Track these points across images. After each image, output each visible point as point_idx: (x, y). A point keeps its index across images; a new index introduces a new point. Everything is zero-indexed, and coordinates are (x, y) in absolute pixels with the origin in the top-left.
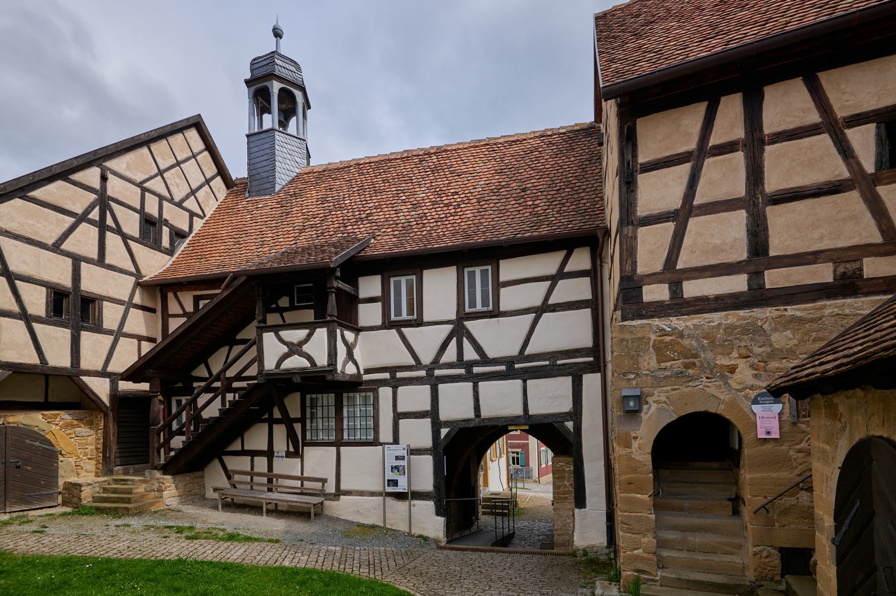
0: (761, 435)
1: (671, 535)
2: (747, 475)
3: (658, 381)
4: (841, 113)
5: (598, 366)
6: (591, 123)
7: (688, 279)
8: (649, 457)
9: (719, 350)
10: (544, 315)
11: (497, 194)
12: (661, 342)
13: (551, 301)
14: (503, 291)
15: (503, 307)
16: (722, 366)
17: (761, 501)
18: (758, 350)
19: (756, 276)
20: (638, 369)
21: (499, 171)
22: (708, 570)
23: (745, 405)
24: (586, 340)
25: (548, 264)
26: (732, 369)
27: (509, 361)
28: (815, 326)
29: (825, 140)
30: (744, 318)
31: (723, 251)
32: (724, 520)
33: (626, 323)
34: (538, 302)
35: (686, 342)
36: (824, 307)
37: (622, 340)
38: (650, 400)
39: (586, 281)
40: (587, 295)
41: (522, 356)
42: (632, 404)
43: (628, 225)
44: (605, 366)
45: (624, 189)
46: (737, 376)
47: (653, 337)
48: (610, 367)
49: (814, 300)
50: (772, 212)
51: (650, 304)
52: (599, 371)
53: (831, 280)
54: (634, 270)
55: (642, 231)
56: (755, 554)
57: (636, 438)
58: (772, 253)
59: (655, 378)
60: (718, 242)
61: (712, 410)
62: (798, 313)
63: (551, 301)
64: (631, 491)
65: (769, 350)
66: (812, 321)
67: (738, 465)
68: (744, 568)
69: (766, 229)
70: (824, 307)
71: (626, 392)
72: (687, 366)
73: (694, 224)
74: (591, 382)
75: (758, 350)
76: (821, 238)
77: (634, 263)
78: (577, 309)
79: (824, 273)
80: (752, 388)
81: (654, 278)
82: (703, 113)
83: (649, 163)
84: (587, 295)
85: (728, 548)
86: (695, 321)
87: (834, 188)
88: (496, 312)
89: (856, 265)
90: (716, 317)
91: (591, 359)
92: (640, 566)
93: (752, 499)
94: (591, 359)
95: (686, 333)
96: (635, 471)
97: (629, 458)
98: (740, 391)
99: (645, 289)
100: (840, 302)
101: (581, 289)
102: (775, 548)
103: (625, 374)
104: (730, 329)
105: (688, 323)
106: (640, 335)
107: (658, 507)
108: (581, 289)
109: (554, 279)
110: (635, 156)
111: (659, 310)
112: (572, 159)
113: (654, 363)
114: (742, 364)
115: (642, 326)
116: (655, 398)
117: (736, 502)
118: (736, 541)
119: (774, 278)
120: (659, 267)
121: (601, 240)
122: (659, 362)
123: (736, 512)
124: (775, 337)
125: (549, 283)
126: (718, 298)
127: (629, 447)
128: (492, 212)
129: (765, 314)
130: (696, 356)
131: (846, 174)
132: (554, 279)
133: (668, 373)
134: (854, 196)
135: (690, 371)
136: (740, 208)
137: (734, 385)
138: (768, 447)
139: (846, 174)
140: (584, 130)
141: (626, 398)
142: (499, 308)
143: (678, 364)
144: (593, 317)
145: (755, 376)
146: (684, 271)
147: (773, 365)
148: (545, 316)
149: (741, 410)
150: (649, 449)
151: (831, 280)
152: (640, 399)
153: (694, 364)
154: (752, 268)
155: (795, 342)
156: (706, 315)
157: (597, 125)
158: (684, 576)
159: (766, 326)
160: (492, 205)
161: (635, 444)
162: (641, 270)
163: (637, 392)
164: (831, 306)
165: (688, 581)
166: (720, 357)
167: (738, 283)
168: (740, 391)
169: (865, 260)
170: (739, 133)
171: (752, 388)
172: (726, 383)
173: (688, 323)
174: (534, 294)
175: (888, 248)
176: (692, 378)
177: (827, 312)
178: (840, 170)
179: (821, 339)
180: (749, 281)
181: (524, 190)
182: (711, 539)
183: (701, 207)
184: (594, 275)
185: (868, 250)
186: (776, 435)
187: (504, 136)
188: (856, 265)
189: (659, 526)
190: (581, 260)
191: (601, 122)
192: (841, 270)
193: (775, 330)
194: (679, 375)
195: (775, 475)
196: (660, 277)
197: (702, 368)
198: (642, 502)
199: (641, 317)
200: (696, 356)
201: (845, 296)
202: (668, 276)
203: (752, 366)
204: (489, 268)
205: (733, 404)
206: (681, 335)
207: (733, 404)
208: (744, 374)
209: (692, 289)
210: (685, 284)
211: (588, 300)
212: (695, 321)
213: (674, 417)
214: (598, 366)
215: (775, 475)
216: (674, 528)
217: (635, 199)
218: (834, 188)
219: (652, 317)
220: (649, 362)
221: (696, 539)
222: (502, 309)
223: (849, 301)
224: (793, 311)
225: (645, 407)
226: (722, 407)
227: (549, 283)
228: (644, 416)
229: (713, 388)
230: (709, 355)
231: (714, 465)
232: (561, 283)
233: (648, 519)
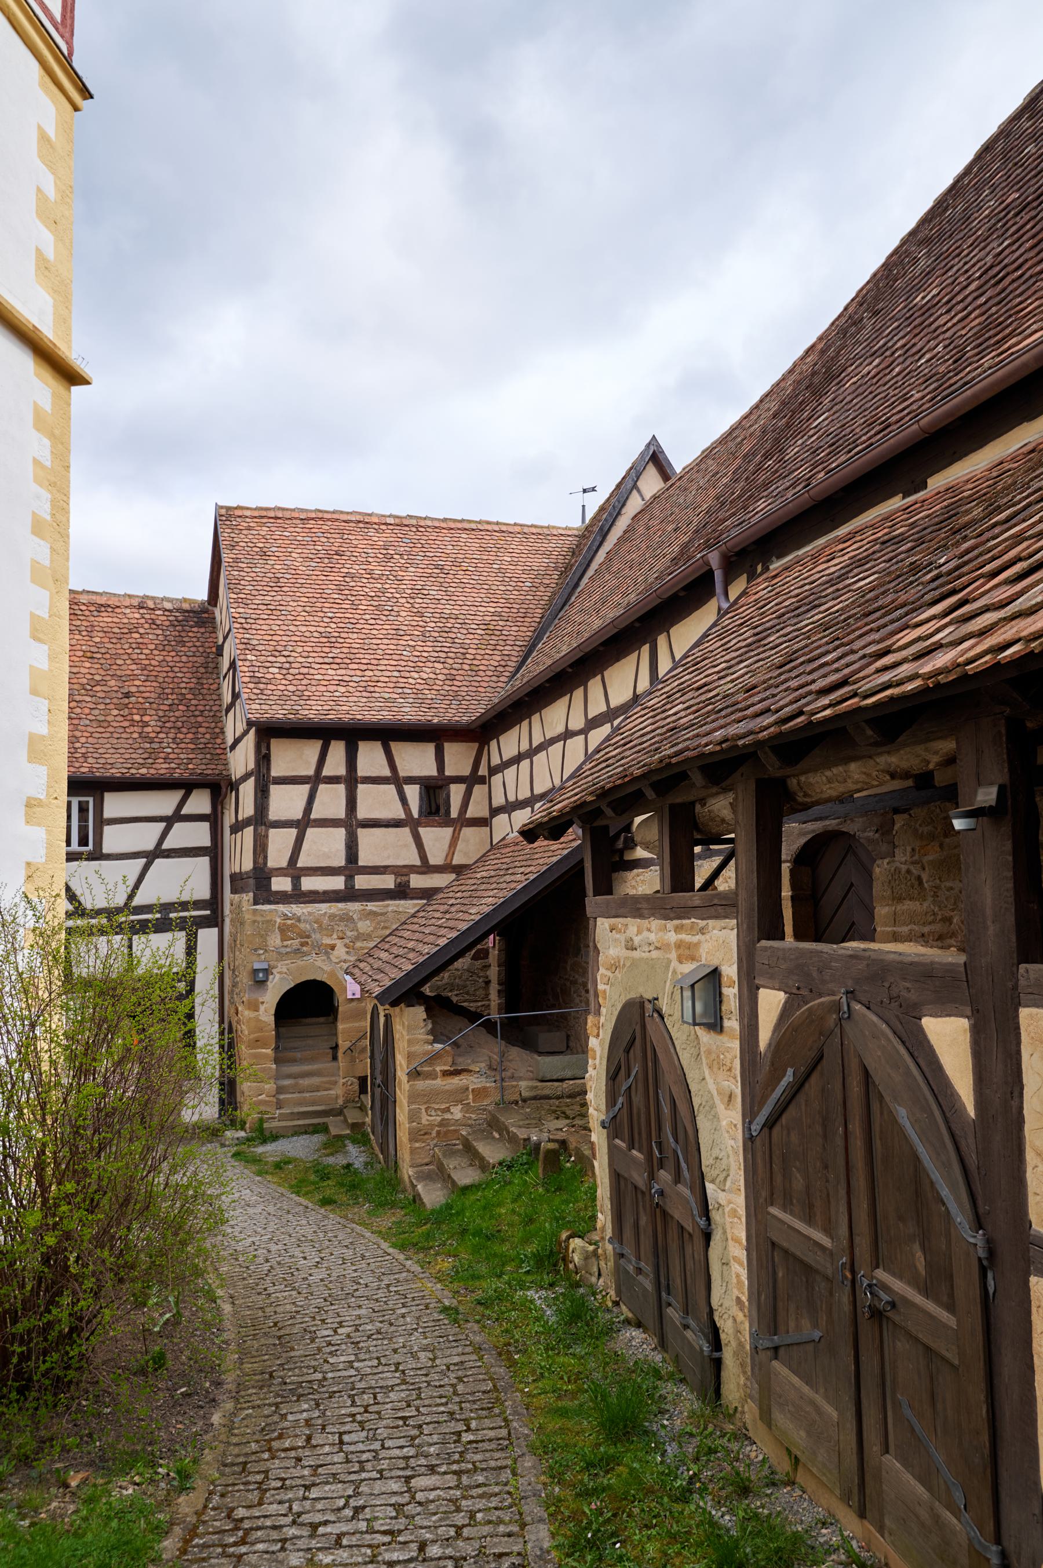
0: (350, 996)
1: (287, 1082)
2: (341, 1026)
3: (281, 956)
4: (402, 773)
5: (215, 920)
6: (203, 603)
7: (305, 875)
8: (273, 1018)
9: (325, 932)
10: (157, 861)
11: (91, 693)
12: (284, 924)
13: (165, 846)
14: (107, 830)
15: (106, 850)
16: (327, 945)
17: (348, 1044)
18: (349, 934)
19: (350, 879)
20: (266, 946)
21: (89, 654)
22: (313, 1104)
23: (340, 974)
24: (204, 892)
25: (164, 803)
26: (333, 947)
27: (110, 913)
28: (383, 918)
29: (392, 788)
30: (342, 910)
31: (329, 857)
32: (327, 1065)
33: (258, 907)
34: (150, 845)
35: (302, 926)
36: (388, 906)
37: (254, 921)
38: (274, 971)
39: (205, 826)
40: (206, 842)
41: (127, 907)
42: (261, 975)
43: (262, 824)
44: (223, 921)
45: (259, 795)
46: (335, 952)
47: (278, 920)
48: (227, 921)
49: (383, 900)
50: (361, 833)
51: (277, 892)
52: (216, 926)
53: (392, 887)
54: (265, 863)
55: (272, 832)
56: (344, 1084)
57: (263, 1003)
58: (360, 863)
59: (279, 953)
60: (326, 850)
61: (319, 979)
62: (374, 909)
63: (165, 846)
64: (258, 1048)
65: (355, 933)
66: (382, 914)
67: (336, 1019)
68: (337, 1097)
69: (357, 845)
70: (388, 906)
71: (257, 966)
72: (302, 945)
73: (311, 833)
74: (208, 937)
75: (349, 934)
76: (389, 857)
77: (266, 858)
78: (195, 856)
79: (388, 882)
80: (345, 961)
81: (280, 872)
82: (319, 749)
83: (279, 777)
84: (206, 842)
85: (327, 1086)
86: (309, 909)
87: (396, 824)
88: (97, 855)
89: (406, 878)
90: (324, 907)
91: (208, 912)
92: (262, 1108)
93: (344, 1044)
94: (208, 912)
95: (302, 918)
96: (261, 1030)
97: (258, 1020)
98: (337, 963)
99: (273, 880)
100: (397, 902)
101: (199, 835)
102: (355, 1077)
103: (256, 950)
104: (332, 917)
105: (304, 911)
106: (268, 918)
107: (276, 1061)
108: (199, 835)
109: (170, 821)
110: (269, 769)
111: (283, 898)
112: (184, 659)
113: (278, 942)
114: (339, 943)
115: (271, 911)
116: (279, 969)
117: (335, 1048)
118: (333, 1079)
119: (362, 882)
120: (284, 864)
121: (224, 790)
122: (282, 940)
123: (335, 1058)
124: (360, 925)
125: (164, 824)
126: (325, 892)
127: (257, 1011)
128: (88, 722)
129: (354, 907)
130: (308, 937)
131: (403, 816)
132: (170, 821)
133: (288, 950)
134: (406, 831)
135: (305, 949)
136: (341, 826)
137: (334, 960)
138: (354, 1004)
139: (403, 816)
140: (194, 612)
141: (256, 971)
142: (101, 849)
143: (296, 943)
144: (211, 866)
145: (347, 953)
146: (302, 869)
147: (359, 944)
148: (158, 862)
149: (338, 978)
150: (273, 1012)
151: (392, 887)
152: (267, 972)
153: (307, 943)
154: (347, 873)
155: (372, 929)
156: (316, 905)
157: (210, 608)
158: (296, 1110)
159: (355, 916)
160: (87, 711)
161: (262, 1008)
162: (271, 864)
163: (265, 966)
164: (393, 905)
165: (298, 1113)
166: (325, 937)
167: (338, 883)
168: (337, 963)
169: (412, 876)
170: (342, 771)
171: (345, 961)
172: (329, 958)
173: (304, 911)
174: (146, 836)
175: (423, 869)
176: (305, 954)
177: (390, 909)
178: (400, 814)
179: (386, 928)
180: (346, 882)
181: (127, 695)
182: (315, 1080)
183: (315, 820)
184: (214, 819)
185: (412, 869)
186: (358, 996)
187: (88, 592)
188: (406, 878)
189: (278, 1077)
190: (200, 803)
191: (216, 606)
192: (399, 880)
193: (360, 919)
194: (297, 951)
195: (357, 1024)
196: (285, 871)
197: (313, 947)
198: (266, 1055)
199: (270, 902)
200: (308, 937)
201: (400, 899)
202: (291, 871)
203: (346, 946)
204: (91, 800)
205: (332, 974)
206: (299, 920)
207: (332, 974)
208: (340, 952)
209: (309, 883)
210: (303, 879)
211: (207, 848)
212: (309, 909)
213: (292, 985)
214: (215, 920)
215: (357, 1024)
216: (289, 1076)
217: (268, 805)
218: (396, 824)
219: (278, 903)
220: (275, 940)
221: (305, 1082)
222: (105, 851)
223: (402, 902)
224: (372, 906)
225: (271, 977)
226: (325, 976)
227: (164, 824)
228: (270, 985)
229: (320, 962)
230: (318, 936)
231: (322, 1020)
232: (177, 826)
233: (270, 1068)
